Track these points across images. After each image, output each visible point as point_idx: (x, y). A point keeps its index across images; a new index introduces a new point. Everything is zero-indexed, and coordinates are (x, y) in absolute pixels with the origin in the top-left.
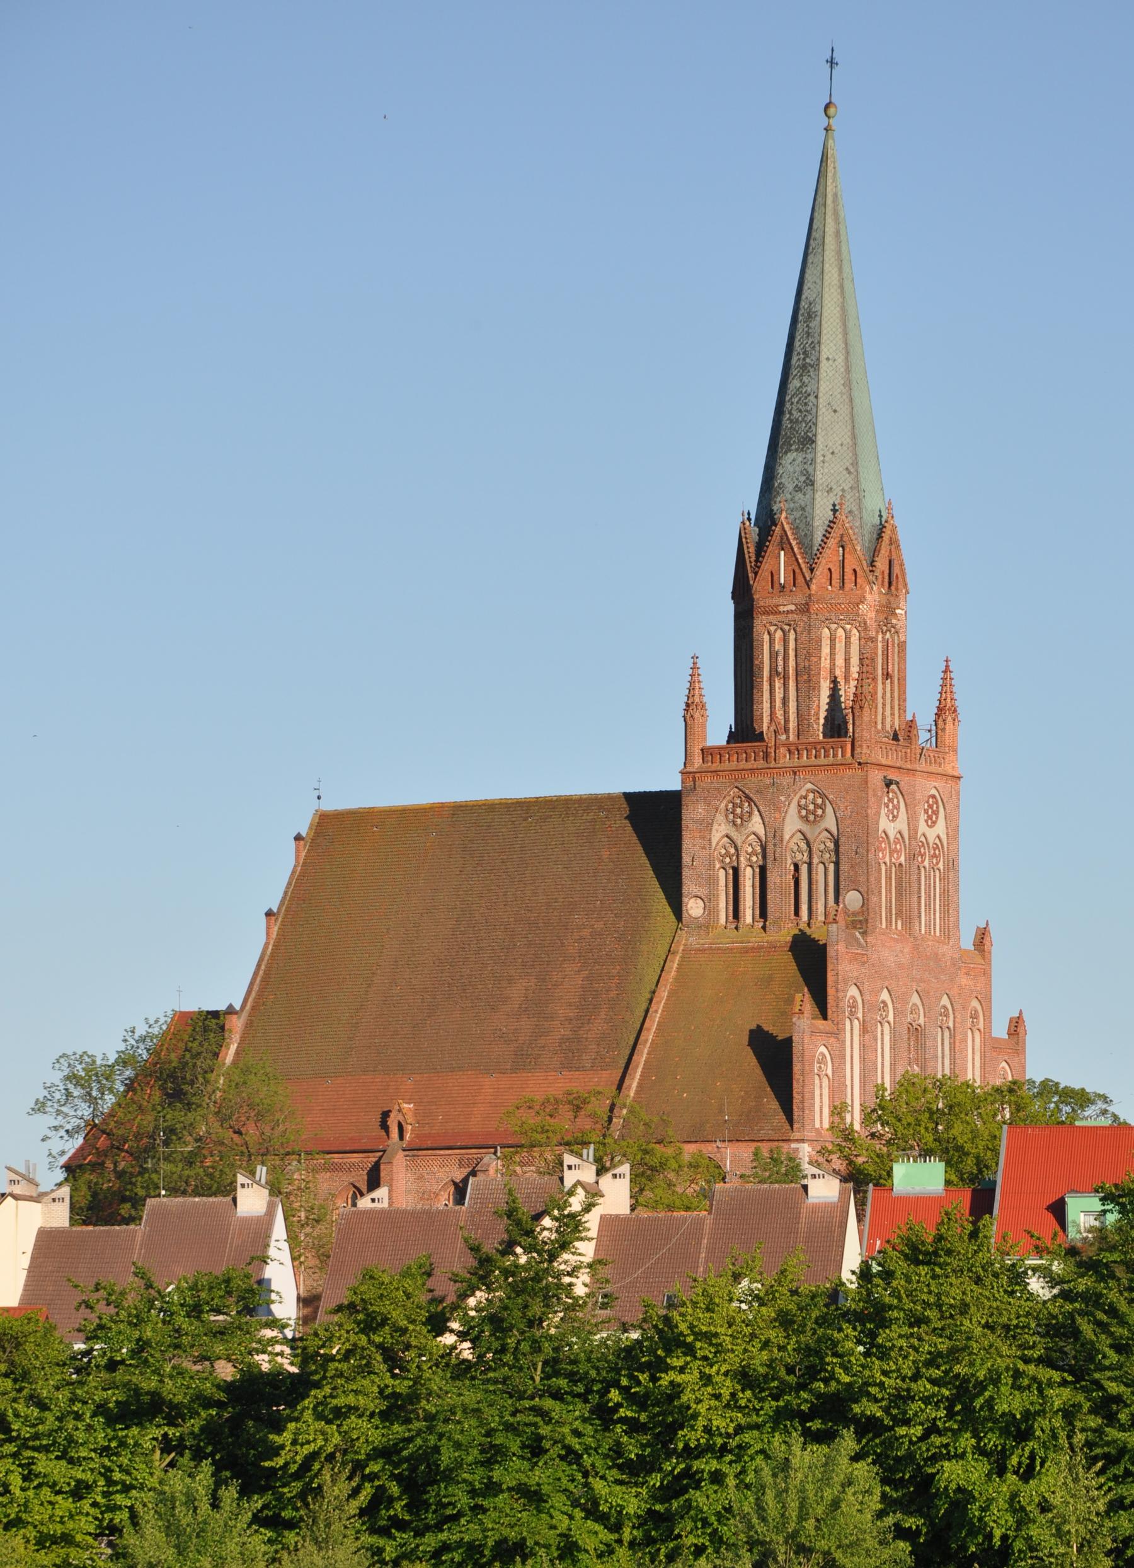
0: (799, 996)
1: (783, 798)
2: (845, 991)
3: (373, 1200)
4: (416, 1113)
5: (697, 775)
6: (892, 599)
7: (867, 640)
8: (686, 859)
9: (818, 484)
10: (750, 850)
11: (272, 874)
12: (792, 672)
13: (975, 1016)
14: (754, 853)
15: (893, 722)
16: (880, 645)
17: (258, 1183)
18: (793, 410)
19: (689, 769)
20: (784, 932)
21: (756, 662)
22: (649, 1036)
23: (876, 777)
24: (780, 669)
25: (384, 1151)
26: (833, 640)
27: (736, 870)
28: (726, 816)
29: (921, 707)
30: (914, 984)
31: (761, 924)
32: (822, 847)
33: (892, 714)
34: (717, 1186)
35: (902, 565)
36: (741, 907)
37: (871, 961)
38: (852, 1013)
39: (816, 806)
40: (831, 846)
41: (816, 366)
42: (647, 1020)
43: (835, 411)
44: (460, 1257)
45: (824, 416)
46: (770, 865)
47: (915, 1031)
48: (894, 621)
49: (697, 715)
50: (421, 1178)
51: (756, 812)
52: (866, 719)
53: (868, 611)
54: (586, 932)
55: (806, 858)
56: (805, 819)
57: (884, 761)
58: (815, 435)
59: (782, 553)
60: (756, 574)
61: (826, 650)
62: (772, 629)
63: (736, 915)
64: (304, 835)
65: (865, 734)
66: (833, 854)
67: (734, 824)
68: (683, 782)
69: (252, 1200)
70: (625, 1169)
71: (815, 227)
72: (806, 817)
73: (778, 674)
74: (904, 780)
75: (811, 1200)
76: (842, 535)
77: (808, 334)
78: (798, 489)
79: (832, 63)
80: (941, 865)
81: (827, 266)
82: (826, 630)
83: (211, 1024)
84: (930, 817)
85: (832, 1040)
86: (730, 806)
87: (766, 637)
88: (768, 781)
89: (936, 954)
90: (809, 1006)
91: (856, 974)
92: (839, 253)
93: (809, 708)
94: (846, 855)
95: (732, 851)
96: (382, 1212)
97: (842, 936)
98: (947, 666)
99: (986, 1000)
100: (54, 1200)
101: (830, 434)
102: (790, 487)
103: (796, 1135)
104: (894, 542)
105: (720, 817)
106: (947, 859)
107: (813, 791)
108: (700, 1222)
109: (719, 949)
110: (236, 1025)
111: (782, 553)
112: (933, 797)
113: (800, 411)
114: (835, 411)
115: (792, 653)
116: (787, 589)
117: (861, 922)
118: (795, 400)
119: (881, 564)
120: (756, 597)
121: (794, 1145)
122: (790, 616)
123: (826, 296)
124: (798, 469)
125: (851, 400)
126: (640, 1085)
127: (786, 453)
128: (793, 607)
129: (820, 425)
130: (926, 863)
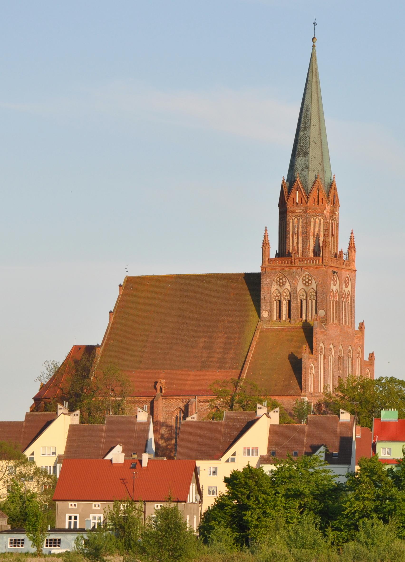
0: (304, 346)
1: (297, 277)
2: (319, 345)
3: (192, 418)
4: (166, 383)
5: (267, 268)
6: (334, 209)
7: (326, 223)
8: (262, 297)
9: (310, 169)
10: (285, 294)
11: (111, 298)
12: (300, 233)
13: (359, 353)
14: (286, 295)
15: (333, 251)
16: (330, 224)
17: (145, 410)
18: (301, 142)
19: (263, 266)
20: (298, 323)
21: (288, 229)
22: (249, 359)
23: (330, 270)
24: (296, 232)
25: (155, 397)
26: (315, 222)
27: (280, 302)
28: (277, 283)
29: (343, 246)
30: (341, 342)
31: (288, 321)
32: (311, 294)
33: (334, 248)
34: (309, 415)
35: (338, 197)
36: (281, 315)
37: (327, 334)
38: (321, 352)
39: (309, 280)
40: (314, 294)
41: (309, 127)
42: (249, 353)
43: (316, 143)
44: (223, 438)
45: (312, 145)
46: (292, 300)
47: (341, 359)
48: (335, 216)
49: (267, 247)
50: (168, 406)
51: (287, 282)
52: (327, 250)
53: (326, 212)
54: (226, 322)
55: (305, 298)
56: (305, 284)
57: (332, 265)
58: (309, 151)
59: (297, 192)
60: (288, 199)
61: (312, 226)
62: (294, 218)
63: (280, 316)
64: (122, 284)
65: (326, 255)
66: (315, 296)
67: (280, 286)
68: (261, 270)
71: (309, 80)
72: (305, 283)
73: (296, 234)
74: (339, 271)
75: (340, 421)
76: (318, 186)
77: (306, 116)
78: (303, 170)
79: (315, 24)
80: (349, 301)
81: (313, 93)
82: (312, 219)
83: (90, 350)
84: (346, 284)
85: (315, 361)
86: (278, 279)
87: (291, 221)
88: (292, 271)
89: (348, 332)
90: (308, 350)
91: (323, 339)
92: (317, 89)
93: (306, 246)
94: (321, 297)
95: (279, 295)
96: (195, 422)
97: (319, 326)
98: (352, 232)
99: (362, 348)
100: (75, 415)
101: (314, 151)
102: (300, 169)
103: (303, 394)
104: (335, 189)
105: (275, 283)
106: (351, 297)
107: (308, 275)
108: (303, 427)
109: (273, 329)
110: (99, 351)
111: (297, 192)
112: (347, 277)
113: (304, 143)
114: (316, 143)
115: (300, 227)
116: (299, 204)
117: (324, 321)
118: (302, 139)
119: (331, 197)
120: (288, 207)
121: (302, 398)
122: (300, 214)
123: (313, 103)
124: (303, 163)
125: (321, 140)
126: (247, 376)
127: (298, 157)
128: (301, 211)
129: (310, 148)
130: (345, 300)
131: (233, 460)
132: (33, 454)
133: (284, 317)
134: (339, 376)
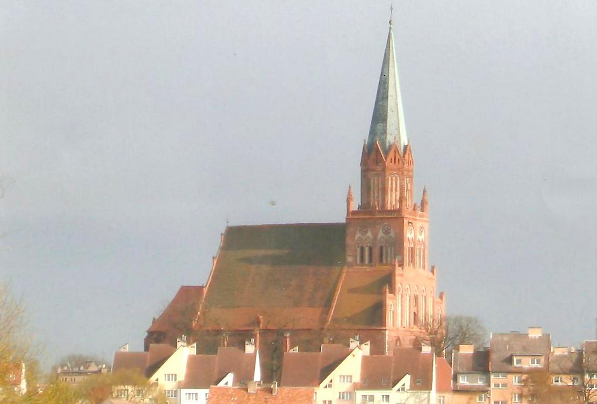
17: (252, 344)
26: (392, 179)
69: (250, 349)
70: (369, 342)
78: (381, 134)
102: (379, 133)
105: (358, 232)
110: (205, 290)
114: (220, 125)
131: (330, 386)
132: (157, 380)
133: (367, 261)
134: (415, 313)
